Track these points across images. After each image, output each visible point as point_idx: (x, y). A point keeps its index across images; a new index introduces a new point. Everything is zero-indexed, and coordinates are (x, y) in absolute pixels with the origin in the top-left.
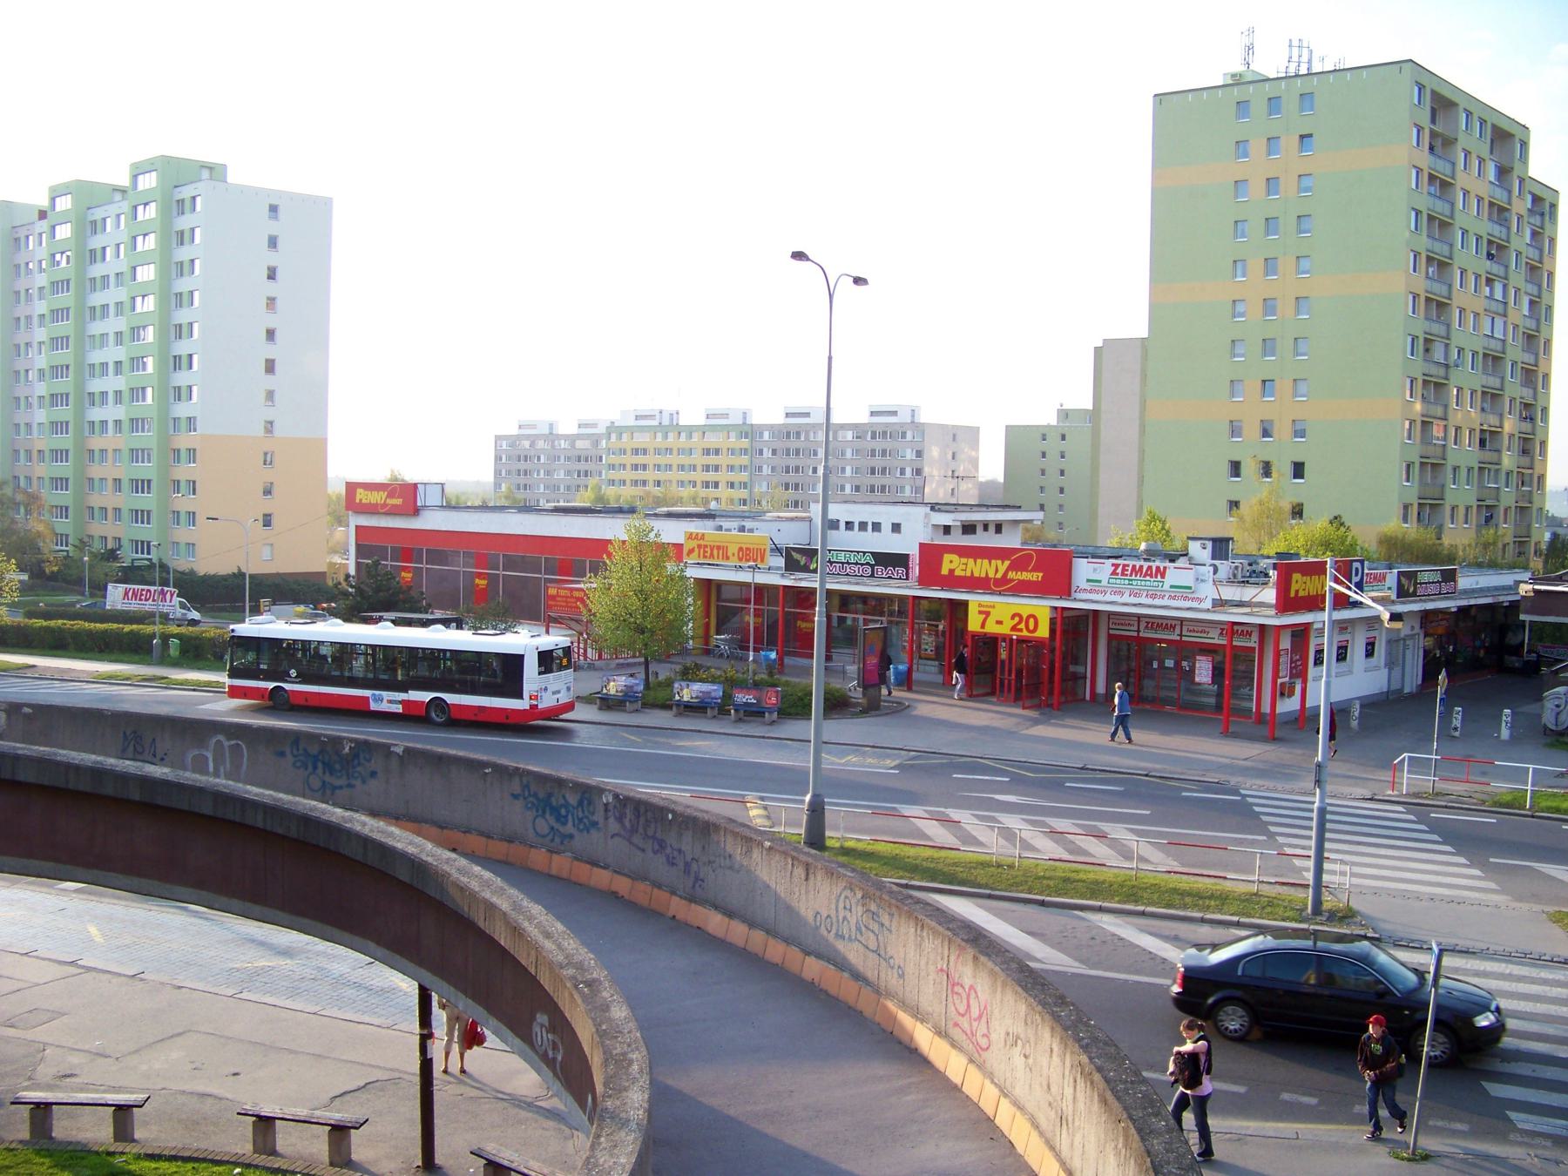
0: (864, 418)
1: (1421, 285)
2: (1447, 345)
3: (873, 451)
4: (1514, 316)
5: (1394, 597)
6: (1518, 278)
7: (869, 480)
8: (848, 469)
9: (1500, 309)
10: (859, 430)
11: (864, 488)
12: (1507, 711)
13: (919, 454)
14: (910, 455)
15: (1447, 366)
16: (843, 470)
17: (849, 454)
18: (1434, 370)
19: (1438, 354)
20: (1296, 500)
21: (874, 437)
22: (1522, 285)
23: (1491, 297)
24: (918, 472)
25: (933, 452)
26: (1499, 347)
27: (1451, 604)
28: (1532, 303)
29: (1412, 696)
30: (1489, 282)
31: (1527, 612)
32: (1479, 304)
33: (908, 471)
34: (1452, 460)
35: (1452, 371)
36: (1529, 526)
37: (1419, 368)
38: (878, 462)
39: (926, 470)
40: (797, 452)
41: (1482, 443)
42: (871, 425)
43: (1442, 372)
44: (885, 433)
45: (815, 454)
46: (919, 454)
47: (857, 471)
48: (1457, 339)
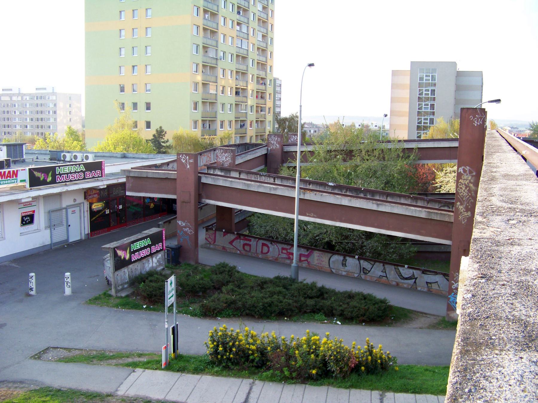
0: (34, 91)
1: (200, 21)
2: (217, 50)
3: (37, 104)
4: (252, 40)
5: (28, 185)
6: (254, 24)
7: (37, 116)
8: (28, 112)
9: (246, 36)
10: (32, 97)
11: (34, 120)
12: (68, 274)
13: (55, 105)
14: (51, 106)
15: (217, 59)
16: (26, 112)
17: (28, 106)
18: (209, 60)
19: (212, 54)
20: (134, 120)
21: (37, 99)
22: (257, 28)
23: (240, 31)
24: (55, 112)
25: (60, 105)
26: (245, 52)
27: (102, 184)
28: (263, 36)
29: (85, 240)
30: (239, 24)
31: (130, 191)
32: (234, 34)
33: (51, 112)
34: (220, 100)
35: (219, 62)
36: (265, 128)
37: (200, 59)
38: (39, 109)
39: (58, 112)
40: (37, 105)
41: (237, 93)
42: (36, 94)
43: (214, 61)
44: (41, 97)
45: (15, 106)
46: (55, 105)
47: (31, 112)
48: (222, 47)
